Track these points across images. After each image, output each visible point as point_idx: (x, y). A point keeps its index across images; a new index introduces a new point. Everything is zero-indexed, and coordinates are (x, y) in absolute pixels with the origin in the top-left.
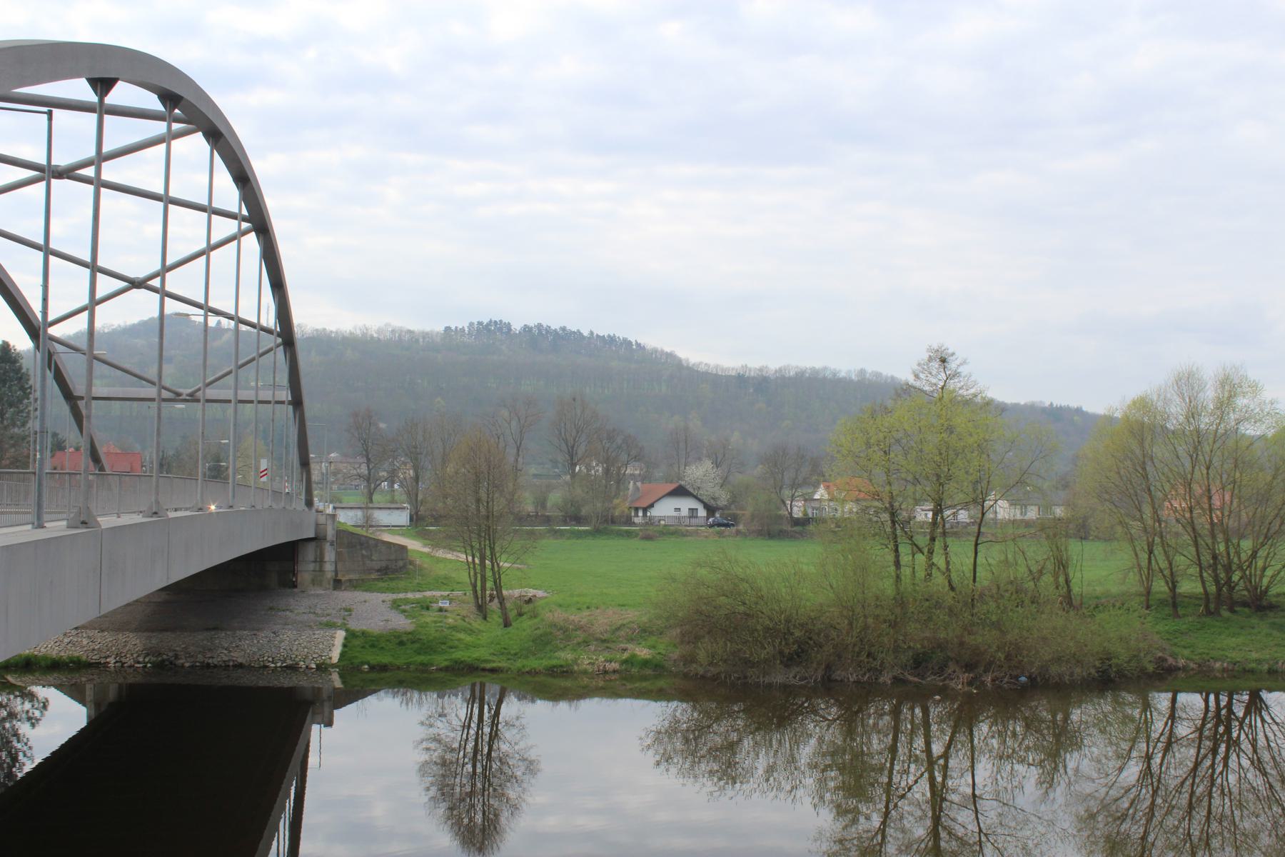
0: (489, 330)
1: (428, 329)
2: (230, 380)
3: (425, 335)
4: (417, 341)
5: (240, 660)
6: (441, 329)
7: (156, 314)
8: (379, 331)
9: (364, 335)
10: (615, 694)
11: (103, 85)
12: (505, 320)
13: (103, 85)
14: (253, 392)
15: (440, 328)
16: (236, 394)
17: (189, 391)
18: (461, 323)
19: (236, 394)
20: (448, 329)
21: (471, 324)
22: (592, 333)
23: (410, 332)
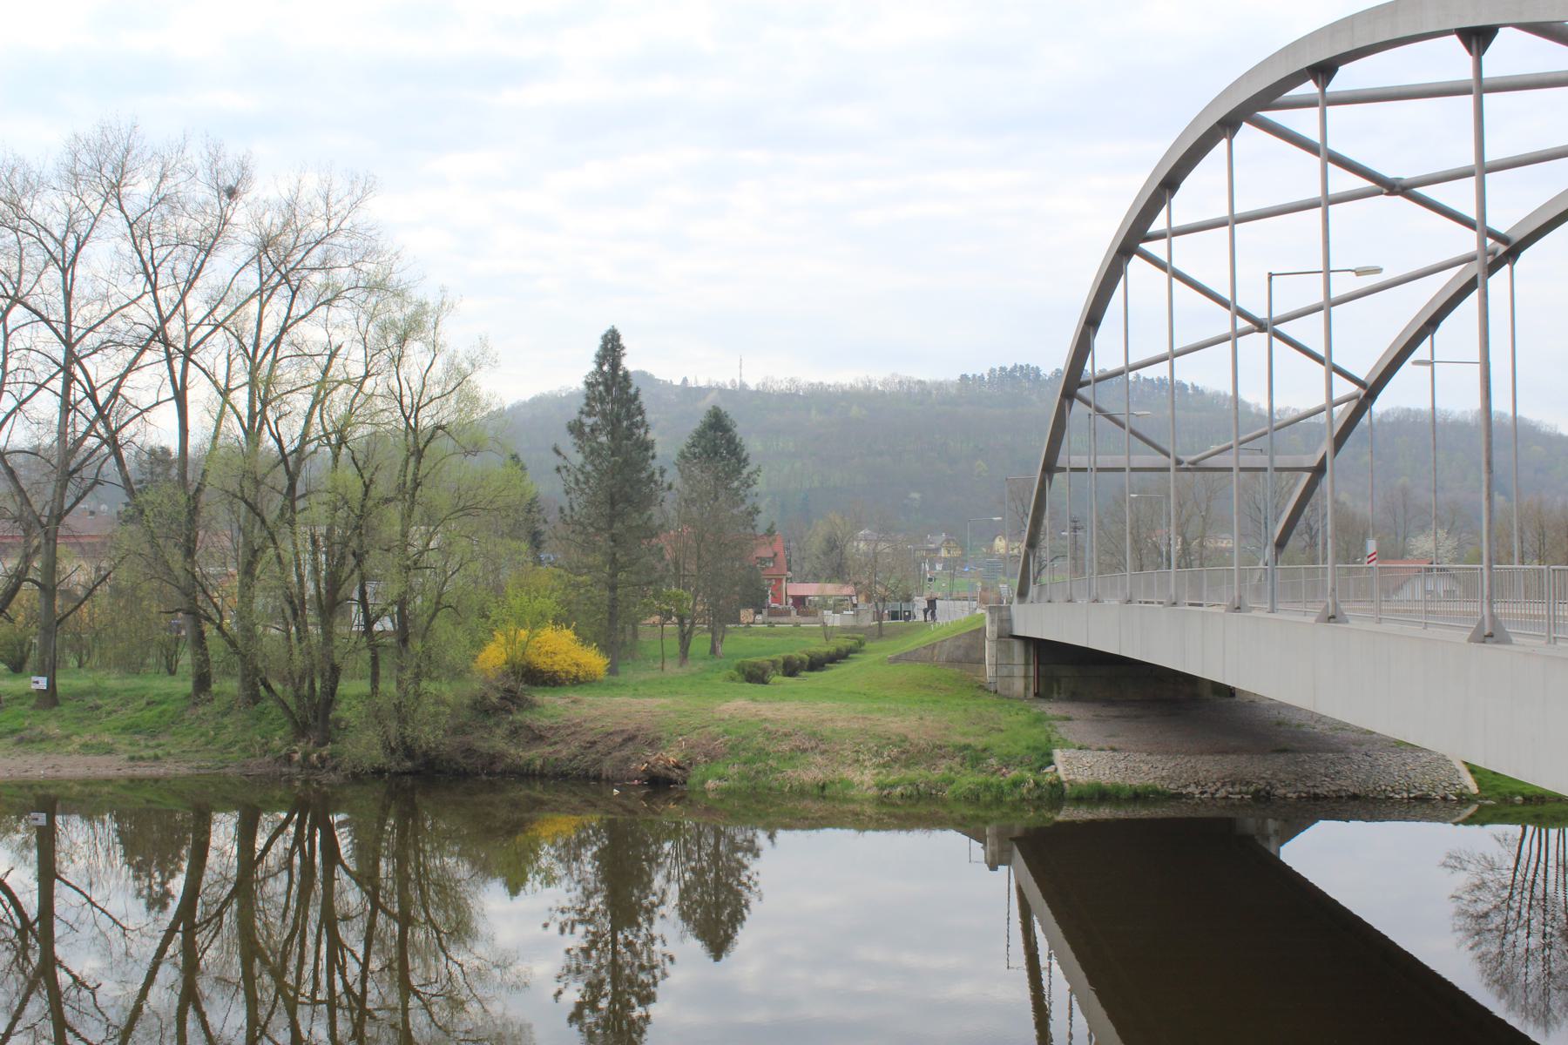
0: (1014, 377)
1: (941, 378)
2: (1263, 443)
3: (939, 386)
4: (930, 393)
5: (1351, 790)
6: (955, 377)
7: (1053, 360)
8: (884, 383)
9: (867, 388)
10: (823, 827)
11: (1477, 38)
12: (1033, 365)
13: (1477, 38)
14: (1266, 458)
15: (955, 377)
16: (1272, 460)
17: (1194, 458)
18: (982, 370)
19: (1272, 460)
20: (964, 377)
21: (992, 371)
22: (685, 380)
23: (920, 382)
